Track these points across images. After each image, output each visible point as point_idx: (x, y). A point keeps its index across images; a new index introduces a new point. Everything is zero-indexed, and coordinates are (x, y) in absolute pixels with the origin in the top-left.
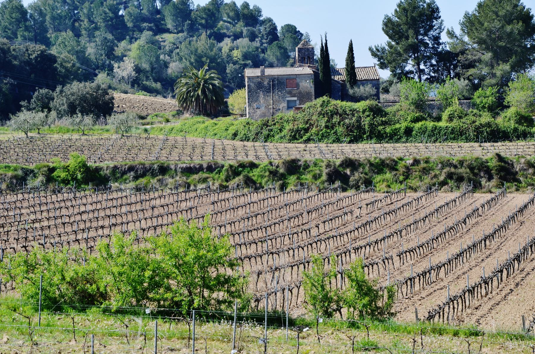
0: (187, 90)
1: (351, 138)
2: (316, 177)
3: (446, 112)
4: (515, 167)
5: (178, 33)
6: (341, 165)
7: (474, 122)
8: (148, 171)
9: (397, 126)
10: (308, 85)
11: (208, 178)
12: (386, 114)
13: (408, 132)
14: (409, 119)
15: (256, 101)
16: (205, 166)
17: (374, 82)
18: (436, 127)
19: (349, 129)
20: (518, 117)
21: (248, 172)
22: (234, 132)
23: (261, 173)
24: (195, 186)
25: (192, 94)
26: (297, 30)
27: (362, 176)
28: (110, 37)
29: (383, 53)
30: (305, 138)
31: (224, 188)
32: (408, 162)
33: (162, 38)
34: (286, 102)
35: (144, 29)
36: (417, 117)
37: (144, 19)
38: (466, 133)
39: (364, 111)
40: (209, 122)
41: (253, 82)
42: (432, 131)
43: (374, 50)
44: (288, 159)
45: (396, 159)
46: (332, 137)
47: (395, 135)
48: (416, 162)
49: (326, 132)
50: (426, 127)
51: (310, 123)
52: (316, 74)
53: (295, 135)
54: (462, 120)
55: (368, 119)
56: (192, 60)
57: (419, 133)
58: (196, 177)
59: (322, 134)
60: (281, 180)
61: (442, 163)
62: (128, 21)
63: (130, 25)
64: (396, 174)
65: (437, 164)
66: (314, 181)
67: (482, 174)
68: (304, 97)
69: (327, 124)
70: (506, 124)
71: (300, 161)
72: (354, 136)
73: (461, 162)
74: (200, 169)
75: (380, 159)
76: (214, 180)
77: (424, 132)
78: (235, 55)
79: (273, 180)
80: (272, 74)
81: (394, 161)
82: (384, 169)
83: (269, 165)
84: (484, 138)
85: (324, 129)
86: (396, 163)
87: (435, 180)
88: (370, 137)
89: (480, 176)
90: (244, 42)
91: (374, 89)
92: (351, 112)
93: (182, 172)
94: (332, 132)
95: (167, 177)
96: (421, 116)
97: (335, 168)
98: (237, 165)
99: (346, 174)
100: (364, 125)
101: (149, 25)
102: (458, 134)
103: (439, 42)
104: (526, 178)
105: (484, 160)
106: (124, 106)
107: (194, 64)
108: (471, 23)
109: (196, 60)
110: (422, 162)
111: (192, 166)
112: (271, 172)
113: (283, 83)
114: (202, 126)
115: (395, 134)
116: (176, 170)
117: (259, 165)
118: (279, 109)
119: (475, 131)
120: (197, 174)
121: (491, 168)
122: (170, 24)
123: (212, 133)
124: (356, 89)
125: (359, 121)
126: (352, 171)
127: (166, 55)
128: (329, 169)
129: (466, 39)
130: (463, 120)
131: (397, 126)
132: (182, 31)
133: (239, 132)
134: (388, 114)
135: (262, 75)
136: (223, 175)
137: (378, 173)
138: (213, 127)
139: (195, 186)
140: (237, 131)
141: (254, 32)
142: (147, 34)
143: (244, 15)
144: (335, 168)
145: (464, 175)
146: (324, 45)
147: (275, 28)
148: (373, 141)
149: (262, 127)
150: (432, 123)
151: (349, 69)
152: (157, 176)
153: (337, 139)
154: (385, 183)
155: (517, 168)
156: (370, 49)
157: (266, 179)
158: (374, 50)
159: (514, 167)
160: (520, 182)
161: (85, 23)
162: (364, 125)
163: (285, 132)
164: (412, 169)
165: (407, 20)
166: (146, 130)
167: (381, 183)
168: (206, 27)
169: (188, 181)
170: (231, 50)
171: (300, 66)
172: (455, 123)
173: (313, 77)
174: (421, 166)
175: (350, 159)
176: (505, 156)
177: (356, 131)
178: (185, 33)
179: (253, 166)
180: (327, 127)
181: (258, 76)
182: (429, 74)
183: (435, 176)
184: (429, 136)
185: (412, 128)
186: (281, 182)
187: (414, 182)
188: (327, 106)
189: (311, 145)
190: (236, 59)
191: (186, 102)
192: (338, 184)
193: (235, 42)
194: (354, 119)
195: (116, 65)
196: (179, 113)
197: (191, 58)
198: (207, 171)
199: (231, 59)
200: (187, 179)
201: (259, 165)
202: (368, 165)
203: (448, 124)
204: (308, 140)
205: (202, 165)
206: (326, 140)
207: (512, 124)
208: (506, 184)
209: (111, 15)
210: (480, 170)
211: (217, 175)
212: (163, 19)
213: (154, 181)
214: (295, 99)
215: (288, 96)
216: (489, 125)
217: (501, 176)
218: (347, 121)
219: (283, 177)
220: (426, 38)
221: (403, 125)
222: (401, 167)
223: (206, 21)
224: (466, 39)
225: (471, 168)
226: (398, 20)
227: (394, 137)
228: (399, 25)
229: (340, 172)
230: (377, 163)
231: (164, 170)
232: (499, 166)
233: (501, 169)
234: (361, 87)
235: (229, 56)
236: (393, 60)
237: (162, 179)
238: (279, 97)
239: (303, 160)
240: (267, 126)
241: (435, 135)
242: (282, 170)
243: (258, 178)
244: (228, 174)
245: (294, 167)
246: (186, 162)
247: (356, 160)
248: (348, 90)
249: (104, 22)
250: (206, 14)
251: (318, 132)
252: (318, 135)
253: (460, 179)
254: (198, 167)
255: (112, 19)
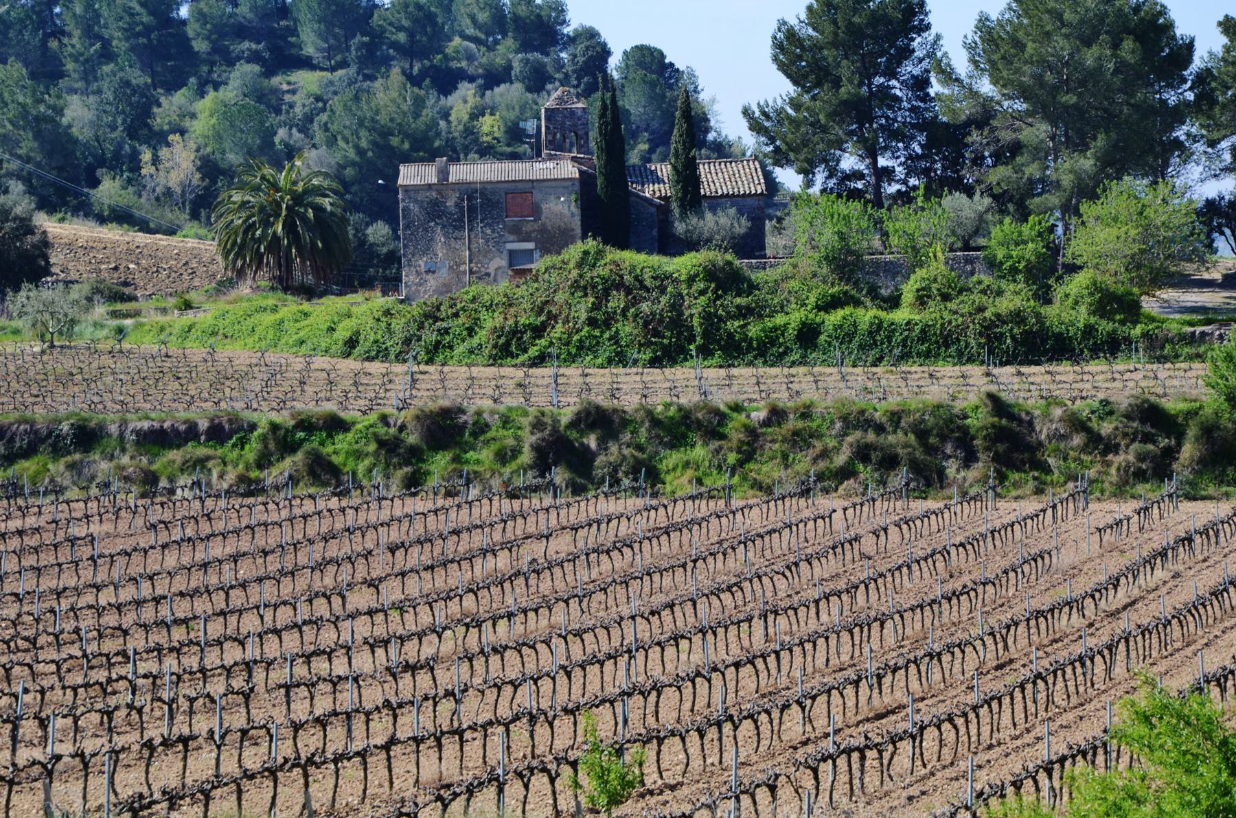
0: (244, 222)
1: (654, 352)
2: (504, 457)
3: (911, 282)
4: (1038, 429)
5: (333, 69)
6: (573, 424)
7: (981, 309)
8: (43, 441)
9: (780, 319)
10: (563, 209)
11: (208, 458)
12: (753, 287)
13: (808, 336)
14: (812, 300)
15: (424, 253)
16: (203, 425)
17: (749, 201)
18: (881, 322)
19: (651, 326)
20: (1098, 296)
21: (322, 444)
22: (348, 334)
23: (356, 447)
24: (171, 480)
25: (258, 232)
26: (667, 61)
27: (626, 452)
28: (139, 78)
29: (780, 123)
30: (533, 351)
31: (249, 488)
32: (754, 415)
33: (289, 83)
34: (505, 255)
35: (239, 58)
36: (833, 296)
37: (242, 32)
38: (958, 340)
39: (691, 280)
40: (292, 306)
41: (416, 201)
42: (870, 333)
43: (757, 114)
44: (432, 406)
45: (722, 407)
46: (607, 350)
47: (773, 345)
48: (777, 415)
49: (590, 336)
50: (855, 325)
51: (549, 312)
52: (586, 180)
53: (508, 344)
54: (949, 305)
55: (703, 300)
56: (364, 144)
57: (837, 338)
58: (175, 455)
59: (580, 341)
60: (407, 463)
61: (845, 419)
62: (198, 35)
63: (201, 46)
64: (721, 448)
65: (832, 422)
66: (498, 466)
67: (949, 449)
68: (553, 241)
69: (592, 314)
70: (1065, 317)
71: (463, 412)
72: (665, 349)
73: (896, 417)
74: (191, 433)
75: (680, 409)
76: (225, 464)
77: (849, 337)
78: (485, 129)
79: (388, 465)
80: (471, 178)
81: (717, 412)
82: (690, 435)
83: (380, 425)
84: (1007, 352)
85: (586, 329)
86: (722, 417)
87: (822, 465)
88: (705, 352)
89: (943, 452)
90: (510, 93)
91: (743, 221)
92: (658, 283)
93: (138, 443)
94: (607, 335)
95: (96, 456)
96: (845, 293)
97: (555, 430)
98: (292, 423)
99: (587, 448)
100: (692, 316)
101: (254, 46)
102: (937, 342)
103: (928, 94)
104: (1065, 459)
105: (955, 411)
106: (132, 266)
107: (370, 154)
108: (994, 43)
109: (374, 143)
110: (791, 416)
111: (166, 425)
112: (382, 443)
113: (498, 202)
114: (269, 319)
115: (773, 342)
116: (121, 436)
117: (354, 423)
118: (488, 275)
119: (981, 334)
120: (178, 447)
121: (972, 431)
122: (310, 42)
123: (295, 337)
124: (694, 220)
125: (676, 305)
126: (602, 442)
127: (294, 130)
128: (539, 435)
129: (986, 87)
130: (951, 305)
131: (780, 319)
132: (343, 64)
133: (362, 337)
134: (757, 287)
135: (440, 183)
136: (251, 452)
137: (672, 446)
138: (297, 321)
139: (171, 480)
140: (358, 333)
141: (544, 65)
142: (244, 72)
143: (516, 19)
144: (555, 430)
145: (900, 451)
146: (608, 102)
147: (605, 53)
148: (716, 359)
149: (423, 323)
150: (873, 312)
151: (680, 167)
152: (69, 453)
153: (617, 354)
154: (690, 473)
155: (1043, 431)
156: (746, 112)
157: (367, 462)
158: (757, 114)
159: (1034, 430)
160: (1047, 470)
161: (75, 41)
162: (692, 316)
163: (482, 336)
164: (764, 434)
165: (836, 34)
166: (120, 330)
167: (678, 473)
168: (409, 51)
169: (154, 467)
170: (476, 114)
171: (551, 158)
172: (933, 313)
173: (577, 187)
174: (791, 429)
175: (598, 408)
176: (1013, 402)
177: (668, 334)
178: (352, 70)
179: (335, 425)
180: (592, 322)
181: (430, 185)
182: (905, 182)
183: (825, 454)
184: (861, 347)
185: (819, 325)
186: (408, 469)
187: (768, 470)
188: (594, 266)
189: (543, 374)
190: (488, 139)
191: (244, 253)
192: (560, 476)
193: (488, 93)
194: (664, 300)
195: (146, 156)
196: (224, 286)
197: (359, 138)
198: (208, 440)
199: (476, 141)
200: (151, 463)
201: (354, 423)
202: (647, 425)
203: (912, 317)
204: (541, 360)
205: (196, 424)
206: (588, 358)
207: (1082, 316)
208: (1015, 476)
209: (146, 19)
210: (943, 438)
211: (236, 452)
212: (294, 32)
213: (57, 468)
214: (531, 246)
215: (512, 238)
216: (1018, 317)
217: (996, 453)
218: (645, 307)
219: (414, 455)
220: (894, 82)
221: (794, 318)
222: (734, 429)
223: (411, 35)
224: (986, 87)
225: (922, 433)
226: (815, 34)
227: (767, 350)
228: (817, 47)
229: (570, 443)
230: (672, 418)
231: (87, 437)
232: (993, 426)
233: (998, 435)
234: (709, 216)
235: (469, 131)
236: (802, 142)
237: (82, 461)
238: (487, 241)
239: (472, 409)
240: (436, 319)
241: (878, 346)
242: (412, 439)
243: (347, 458)
244: (266, 447)
245: (446, 429)
246: (153, 415)
247: (615, 411)
248: (673, 223)
249: (127, 39)
250: (409, 16)
251: (570, 335)
252: (568, 344)
253: (889, 462)
254: (183, 428)
255: (148, 30)
